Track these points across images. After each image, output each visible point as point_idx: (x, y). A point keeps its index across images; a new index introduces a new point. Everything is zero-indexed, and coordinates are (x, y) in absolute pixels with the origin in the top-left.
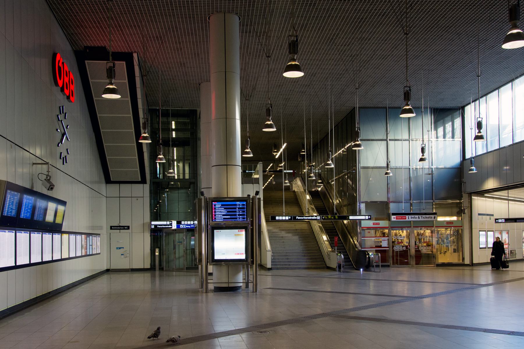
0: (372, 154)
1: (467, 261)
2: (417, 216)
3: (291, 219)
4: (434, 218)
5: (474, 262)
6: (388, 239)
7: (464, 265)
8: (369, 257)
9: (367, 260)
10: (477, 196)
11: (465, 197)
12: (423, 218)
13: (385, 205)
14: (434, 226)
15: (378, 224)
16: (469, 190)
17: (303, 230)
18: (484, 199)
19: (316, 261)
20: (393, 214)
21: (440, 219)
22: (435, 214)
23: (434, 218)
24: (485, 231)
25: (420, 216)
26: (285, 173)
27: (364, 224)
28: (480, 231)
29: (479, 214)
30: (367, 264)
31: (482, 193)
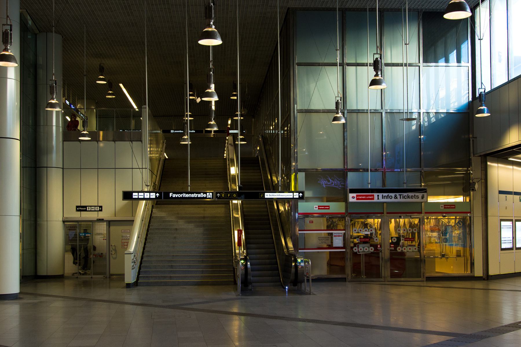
0: (318, 90)
1: (479, 272)
2: (393, 195)
3: (160, 197)
4: (423, 198)
5: (491, 272)
6: (345, 234)
7: (472, 278)
8: (296, 266)
9: (293, 270)
10: (498, 162)
11: (476, 161)
12: (404, 197)
13: (342, 174)
14: (423, 211)
15: (328, 208)
16: (482, 149)
17: (215, 217)
18: (510, 167)
19: (219, 271)
20: (352, 191)
21: (431, 199)
22: (424, 191)
23: (423, 198)
24: (511, 220)
25: (398, 194)
26: (237, 129)
27: (303, 207)
28: (502, 220)
29: (501, 192)
30: (292, 277)
31: (504, 156)
